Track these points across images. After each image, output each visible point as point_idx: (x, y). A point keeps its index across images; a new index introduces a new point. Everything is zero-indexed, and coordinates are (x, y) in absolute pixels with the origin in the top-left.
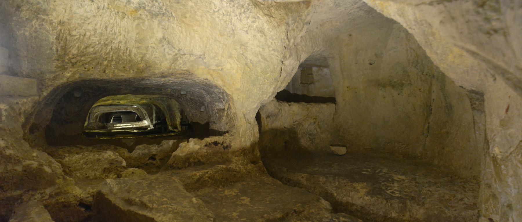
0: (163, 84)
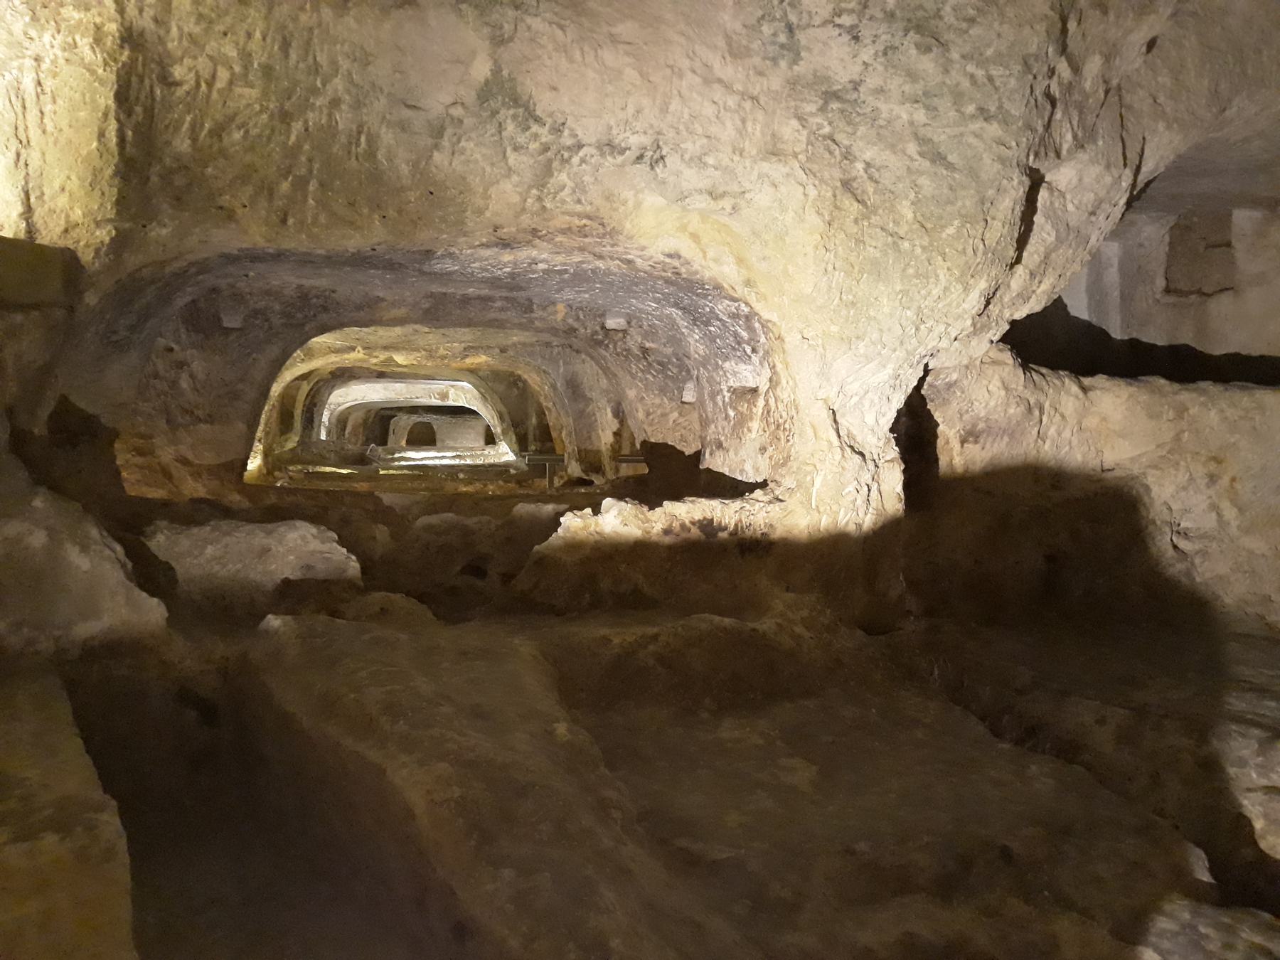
0: (512, 275)
